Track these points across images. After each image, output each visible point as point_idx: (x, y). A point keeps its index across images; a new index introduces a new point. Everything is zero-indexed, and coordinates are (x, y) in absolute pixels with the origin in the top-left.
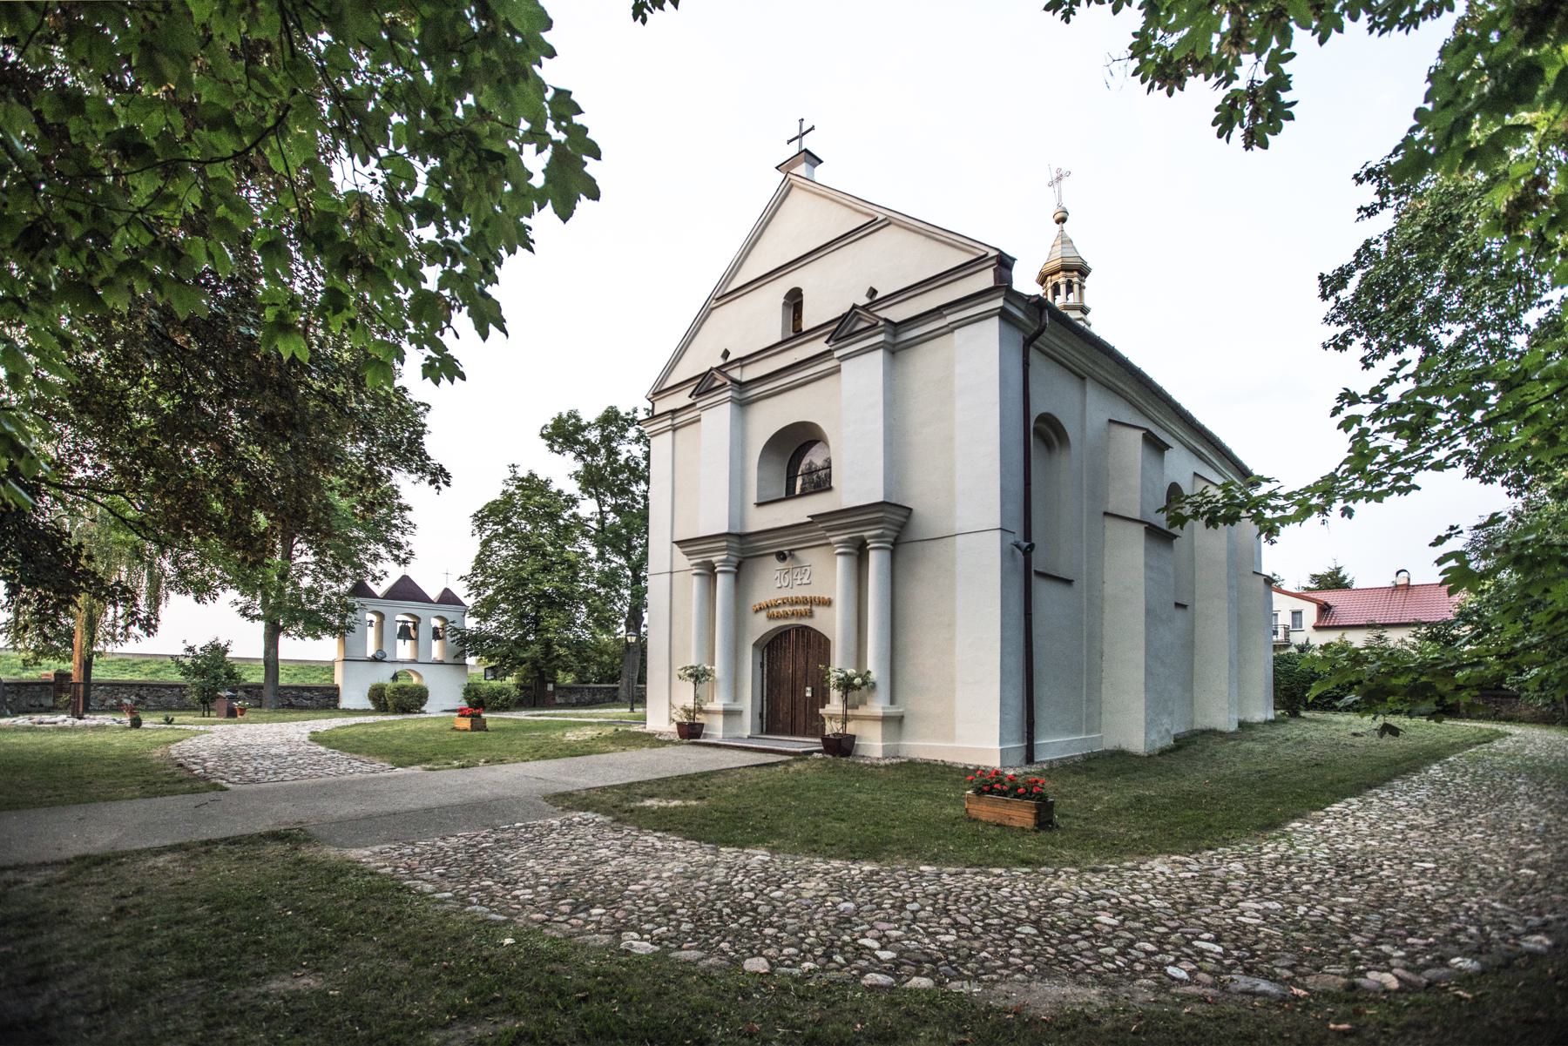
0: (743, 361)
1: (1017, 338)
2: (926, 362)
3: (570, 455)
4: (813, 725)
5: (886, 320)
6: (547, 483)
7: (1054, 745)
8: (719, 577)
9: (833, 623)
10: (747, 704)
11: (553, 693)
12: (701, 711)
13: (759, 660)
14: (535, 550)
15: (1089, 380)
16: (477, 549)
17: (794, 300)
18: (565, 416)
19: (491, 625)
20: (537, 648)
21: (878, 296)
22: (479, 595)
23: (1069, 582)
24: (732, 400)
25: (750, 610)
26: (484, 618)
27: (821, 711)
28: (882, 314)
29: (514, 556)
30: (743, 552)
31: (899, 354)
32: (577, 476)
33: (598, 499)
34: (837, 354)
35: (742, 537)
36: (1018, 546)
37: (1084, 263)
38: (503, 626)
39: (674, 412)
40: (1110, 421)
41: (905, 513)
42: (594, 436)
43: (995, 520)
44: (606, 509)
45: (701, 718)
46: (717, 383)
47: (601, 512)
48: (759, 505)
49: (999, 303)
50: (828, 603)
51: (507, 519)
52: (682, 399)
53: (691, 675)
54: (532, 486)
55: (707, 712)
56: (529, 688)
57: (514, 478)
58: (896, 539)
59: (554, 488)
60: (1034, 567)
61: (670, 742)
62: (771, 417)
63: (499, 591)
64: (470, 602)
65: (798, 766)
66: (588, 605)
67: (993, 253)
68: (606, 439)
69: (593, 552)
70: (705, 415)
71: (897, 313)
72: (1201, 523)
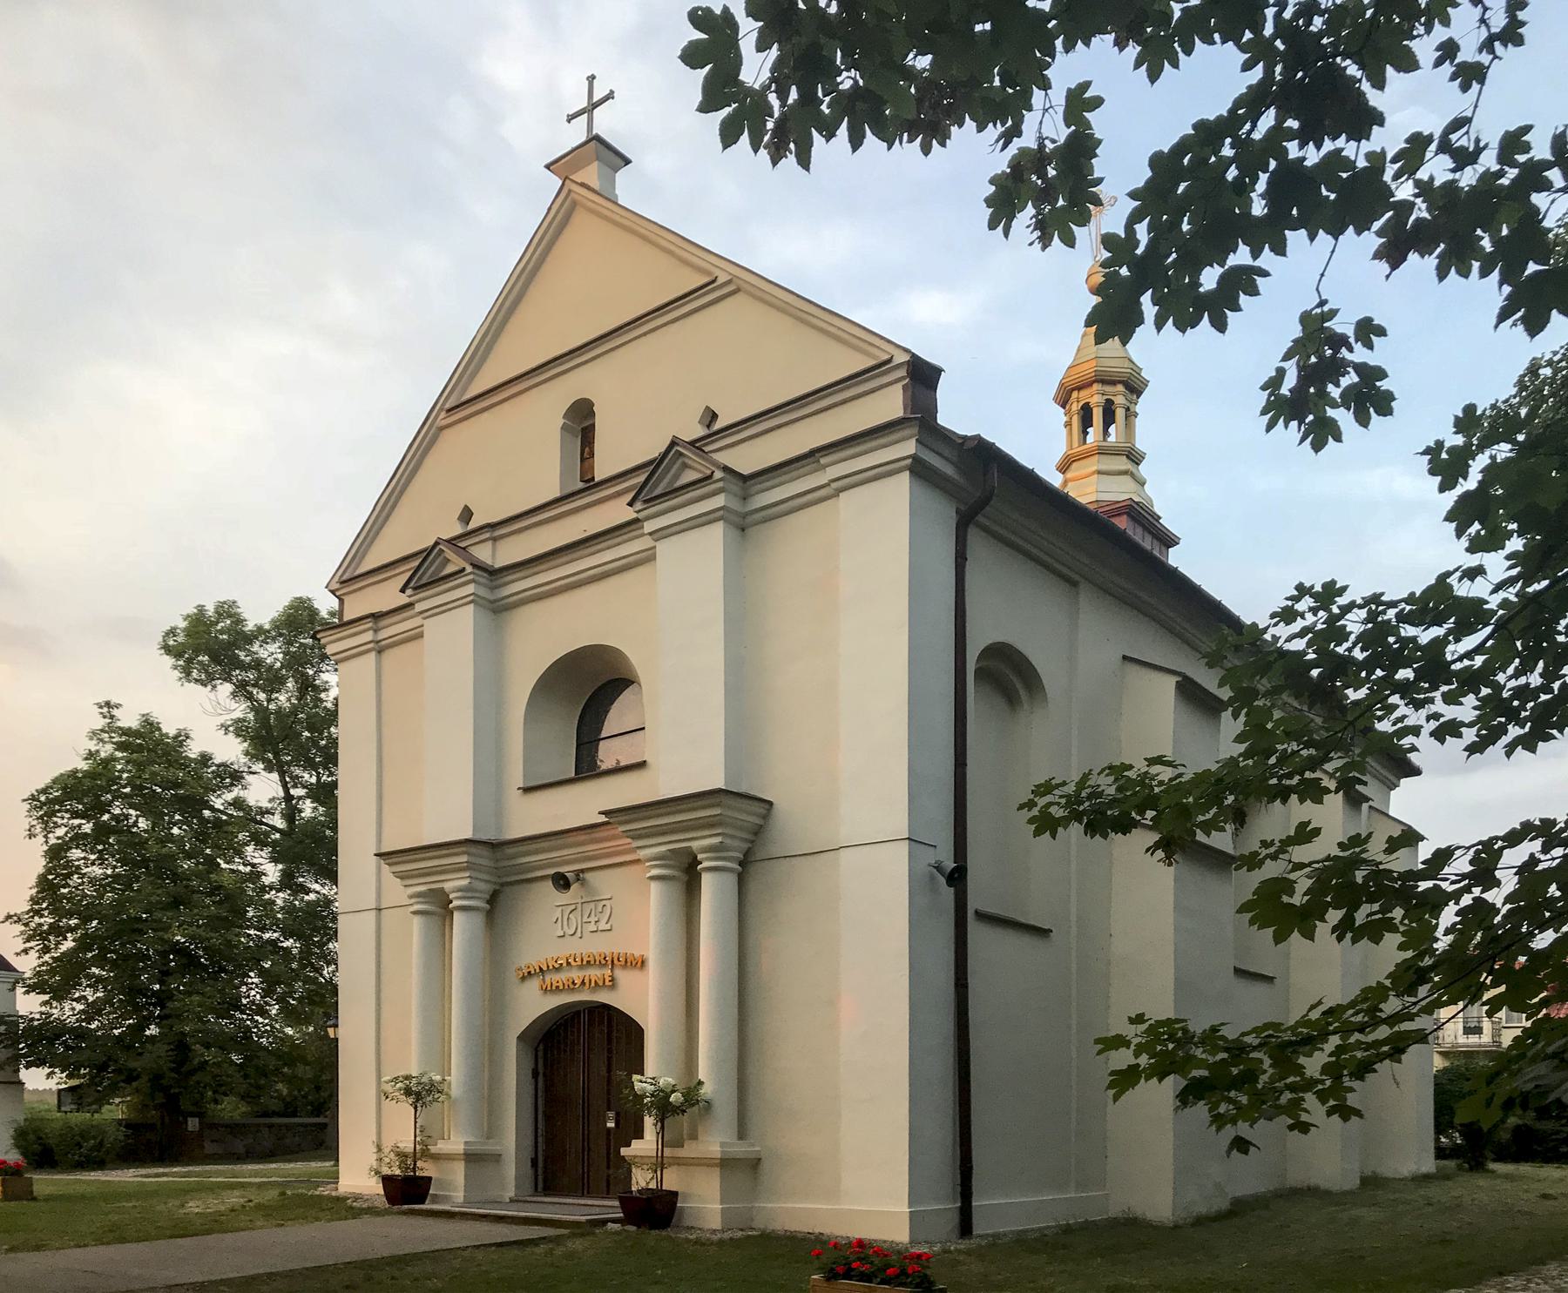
0: (495, 530)
1: (944, 514)
2: (796, 544)
3: (226, 689)
4: (613, 1175)
5: (726, 469)
6: (181, 738)
7: (1005, 1206)
8: (456, 915)
9: (644, 999)
10: (510, 1140)
11: (200, 1135)
12: (426, 1154)
13: (531, 1065)
14: (163, 868)
15: (1083, 586)
16: (39, 865)
17: (582, 422)
18: (210, 610)
19: (68, 1012)
20: (162, 1050)
21: (717, 426)
22: (46, 950)
23: (1043, 933)
24: (476, 600)
25: (513, 977)
26: (59, 993)
27: (624, 1151)
28: (724, 458)
29: (116, 877)
30: (498, 875)
31: (751, 531)
32: (239, 728)
33: (282, 774)
34: (649, 526)
35: (495, 846)
36: (939, 868)
37: (1138, 370)
38: (93, 1011)
39: (376, 617)
40: (1125, 658)
41: (759, 809)
42: (271, 653)
43: (899, 824)
44: (298, 792)
45: (426, 1169)
46: (450, 569)
47: (288, 798)
48: (527, 790)
49: (909, 447)
50: (641, 964)
51: (104, 808)
52: (387, 595)
53: (408, 1092)
54: (150, 748)
55: (437, 1157)
56: (151, 1127)
57: (110, 729)
58: (747, 853)
59: (193, 750)
60: (973, 904)
61: (372, 1211)
62: (548, 633)
63: (83, 944)
64: (27, 964)
65: (577, 1245)
66: (262, 973)
67: (901, 358)
68: (296, 662)
69: (272, 873)
70: (431, 626)
71: (748, 457)
72: (1076, 829)
